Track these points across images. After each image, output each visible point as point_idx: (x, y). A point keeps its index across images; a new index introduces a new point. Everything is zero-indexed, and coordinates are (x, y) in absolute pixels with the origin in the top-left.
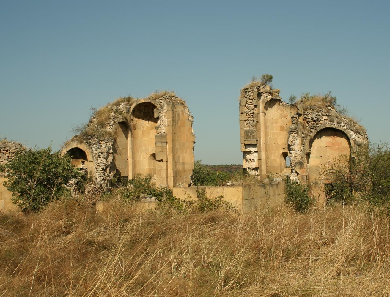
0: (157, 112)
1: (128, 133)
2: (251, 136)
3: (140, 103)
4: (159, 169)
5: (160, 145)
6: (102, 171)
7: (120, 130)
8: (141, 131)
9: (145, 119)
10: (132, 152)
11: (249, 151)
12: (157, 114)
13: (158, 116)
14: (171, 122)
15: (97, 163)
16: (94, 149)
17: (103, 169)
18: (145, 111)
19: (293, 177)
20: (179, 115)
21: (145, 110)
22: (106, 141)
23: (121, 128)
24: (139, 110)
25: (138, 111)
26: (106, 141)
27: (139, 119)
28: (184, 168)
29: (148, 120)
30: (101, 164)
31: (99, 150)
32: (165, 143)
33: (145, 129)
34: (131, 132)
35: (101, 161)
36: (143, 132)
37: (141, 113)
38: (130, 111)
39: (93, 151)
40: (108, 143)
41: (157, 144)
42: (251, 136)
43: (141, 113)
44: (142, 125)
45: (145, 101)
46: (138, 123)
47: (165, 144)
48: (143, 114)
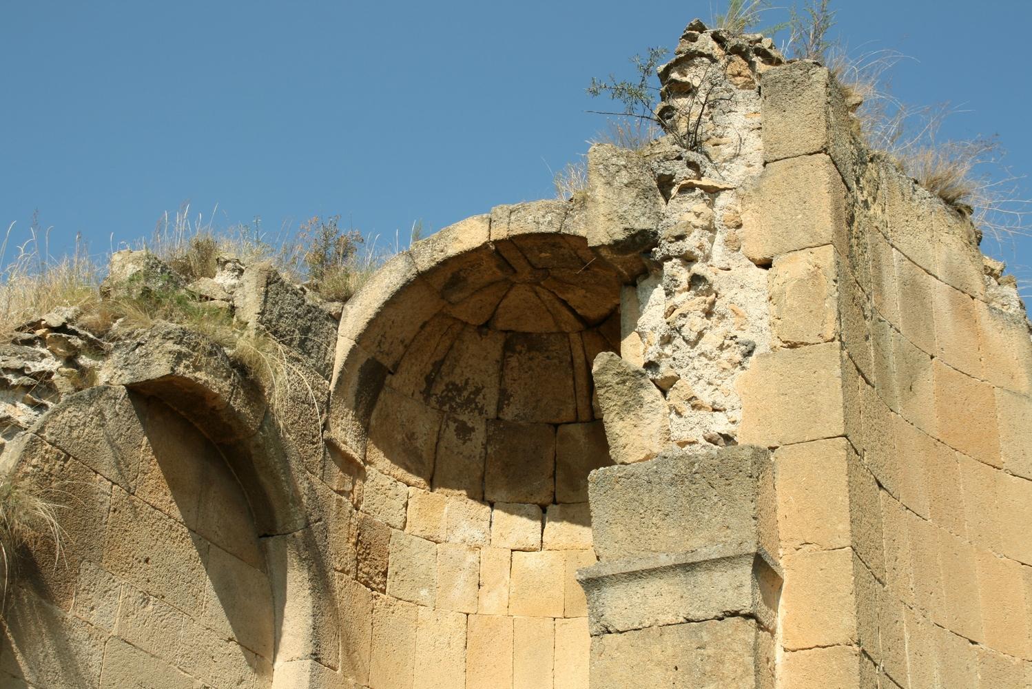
0: (624, 177)
1: (276, 598)
3: (440, 257)
5: (661, 601)
7: (155, 492)
8: (452, 623)
9: (500, 495)
12: (629, 196)
13: (643, 224)
14: (829, 287)
18: (509, 414)
20: (914, 292)
21: (504, 397)
23: (174, 483)
24: (439, 389)
25: (427, 394)
27: (432, 484)
29: (544, 509)
32: (745, 573)
33: (492, 603)
34: (321, 584)
36: (474, 633)
37: (464, 431)
38: (331, 340)
41: (619, 604)
43: (464, 431)
44: (471, 558)
46: (417, 524)
47: (735, 586)
48: (479, 436)
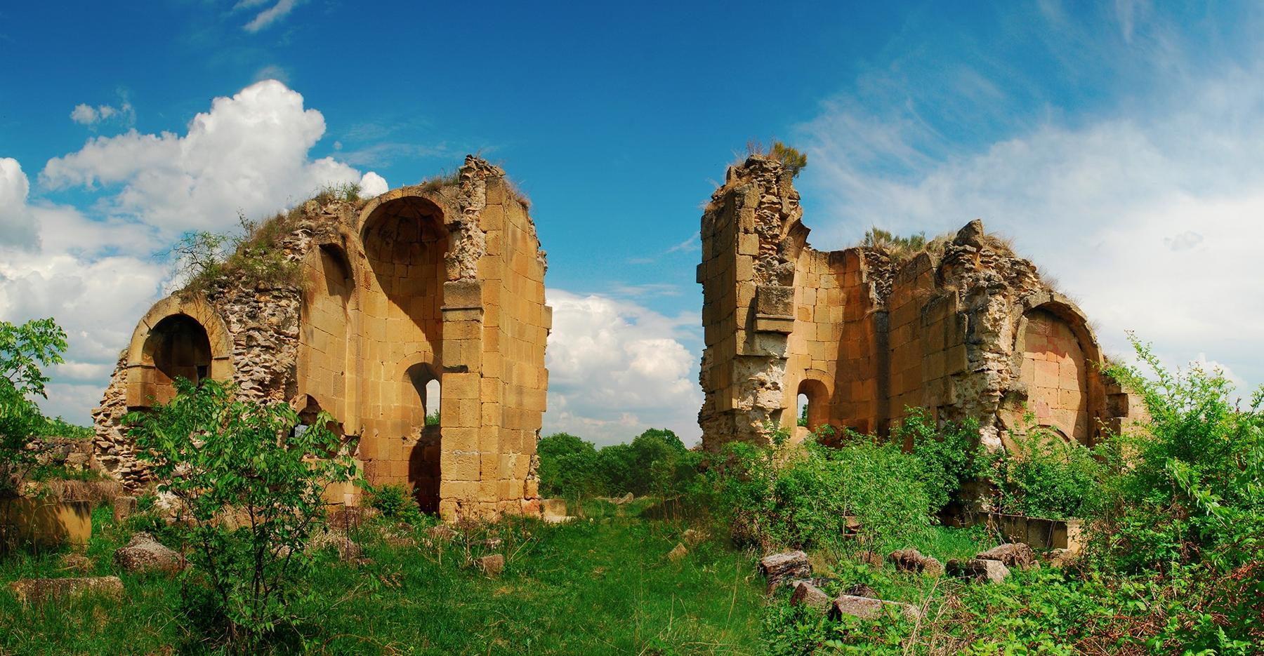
2: (780, 307)
4: (454, 397)
6: (259, 390)
10: (358, 354)
11: (762, 353)
15: (243, 362)
16: (233, 318)
17: (261, 383)
19: (664, 455)
21: (398, 234)
22: (276, 293)
26: (276, 293)
28: (520, 404)
30: (256, 368)
31: (252, 324)
35: (257, 360)
37: (388, 244)
39: (228, 323)
40: (284, 302)
42: (780, 307)
43: (388, 244)
45: (405, 195)
